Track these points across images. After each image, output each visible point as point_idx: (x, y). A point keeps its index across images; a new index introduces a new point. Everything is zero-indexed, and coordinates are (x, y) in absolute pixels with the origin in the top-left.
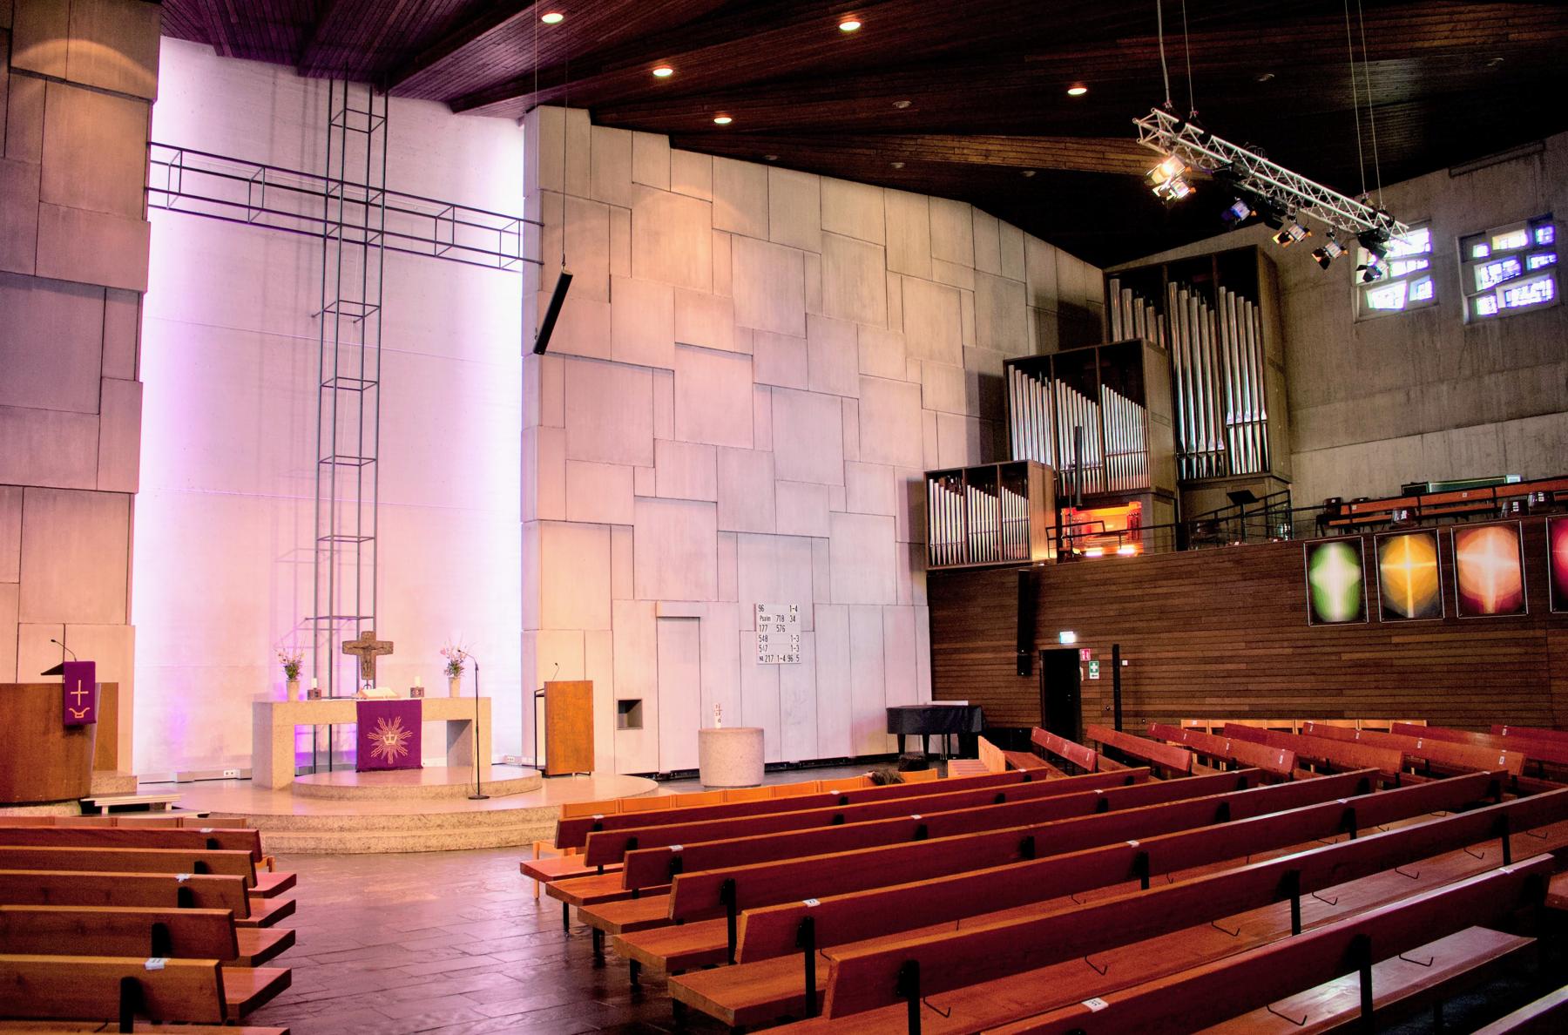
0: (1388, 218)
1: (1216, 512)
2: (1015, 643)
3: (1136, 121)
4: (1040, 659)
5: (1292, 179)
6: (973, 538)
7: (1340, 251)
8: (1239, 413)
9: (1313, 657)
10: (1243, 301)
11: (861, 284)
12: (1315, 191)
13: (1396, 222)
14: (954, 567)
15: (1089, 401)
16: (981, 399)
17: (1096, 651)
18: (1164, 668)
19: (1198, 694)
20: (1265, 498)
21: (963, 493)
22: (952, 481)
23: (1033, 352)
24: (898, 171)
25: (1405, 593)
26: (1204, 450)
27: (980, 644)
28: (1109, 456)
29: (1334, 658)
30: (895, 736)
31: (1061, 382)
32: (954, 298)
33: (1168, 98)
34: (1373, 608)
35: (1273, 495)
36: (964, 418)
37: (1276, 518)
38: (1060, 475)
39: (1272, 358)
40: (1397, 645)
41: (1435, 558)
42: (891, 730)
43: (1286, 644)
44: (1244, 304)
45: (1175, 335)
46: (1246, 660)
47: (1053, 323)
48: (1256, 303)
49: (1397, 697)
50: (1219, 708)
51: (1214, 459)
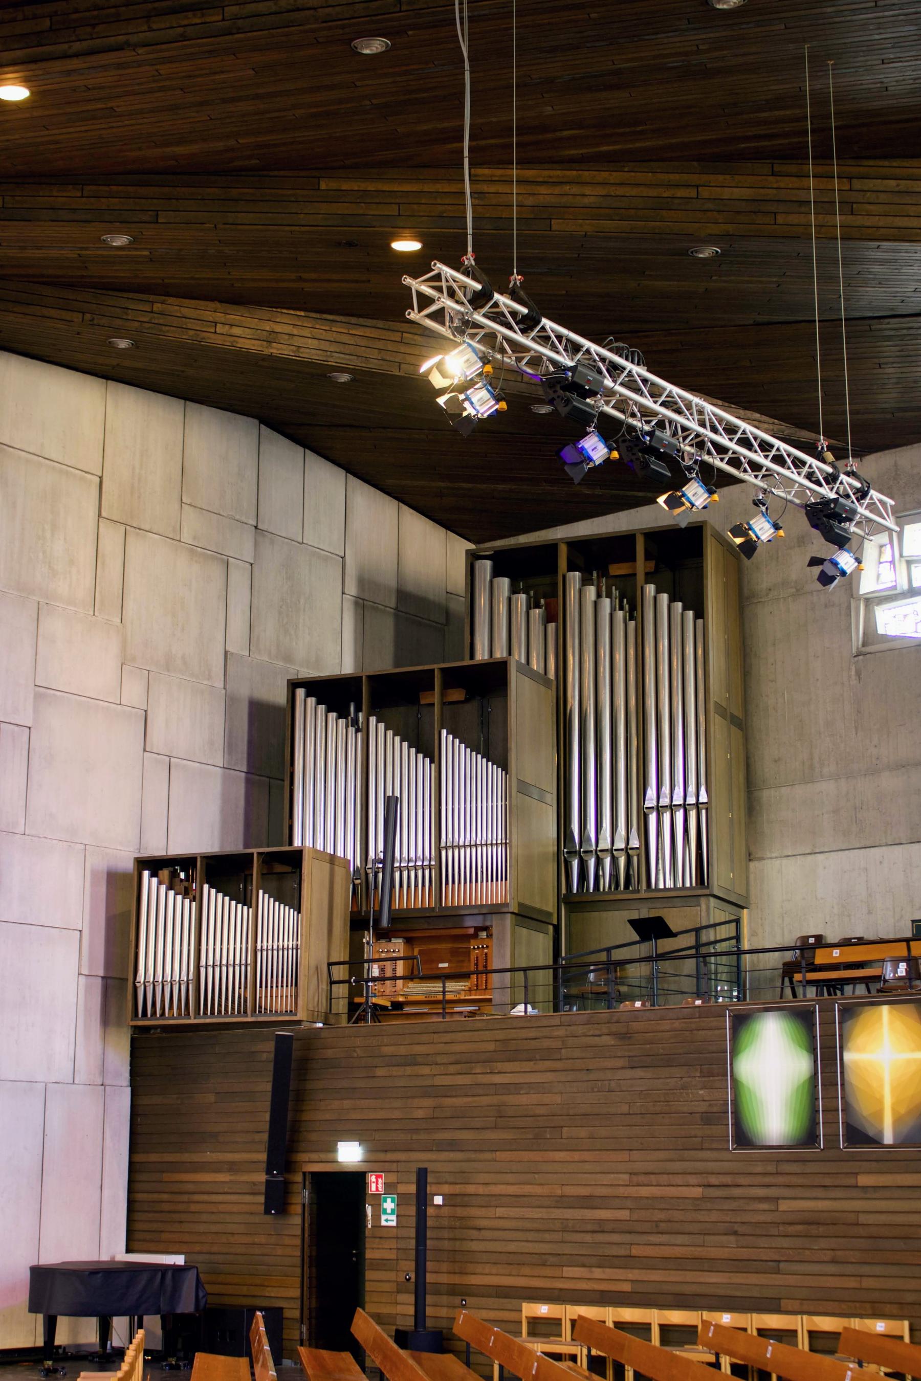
0: (858, 485)
1: (608, 950)
2: (263, 1157)
3: (408, 281)
4: (304, 1188)
5: (689, 406)
6: (208, 976)
7: (772, 530)
8: (666, 789)
9: (734, 1205)
10: (680, 610)
12: (731, 430)
13: (872, 492)
16: (250, 743)
17: (393, 1178)
18: (500, 1212)
19: (552, 1260)
21: (197, 899)
22: (182, 875)
23: (348, 667)
24: (123, 353)
25: (880, 1101)
26: (609, 846)
27: (210, 1156)
28: (446, 848)
30: (40, 1317)
31: (378, 721)
32: (216, 571)
33: (470, 249)
34: (831, 1123)
35: (715, 925)
36: (243, 775)
37: (716, 964)
38: (367, 874)
40: (865, 1188)
42: (34, 1307)
43: (693, 1180)
44: (682, 614)
45: (572, 661)
46: (629, 1204)
47: (386, 628)
48: (700, 614)
49: (864, 1279)
50: (584, 1286)
51: (622, 861)
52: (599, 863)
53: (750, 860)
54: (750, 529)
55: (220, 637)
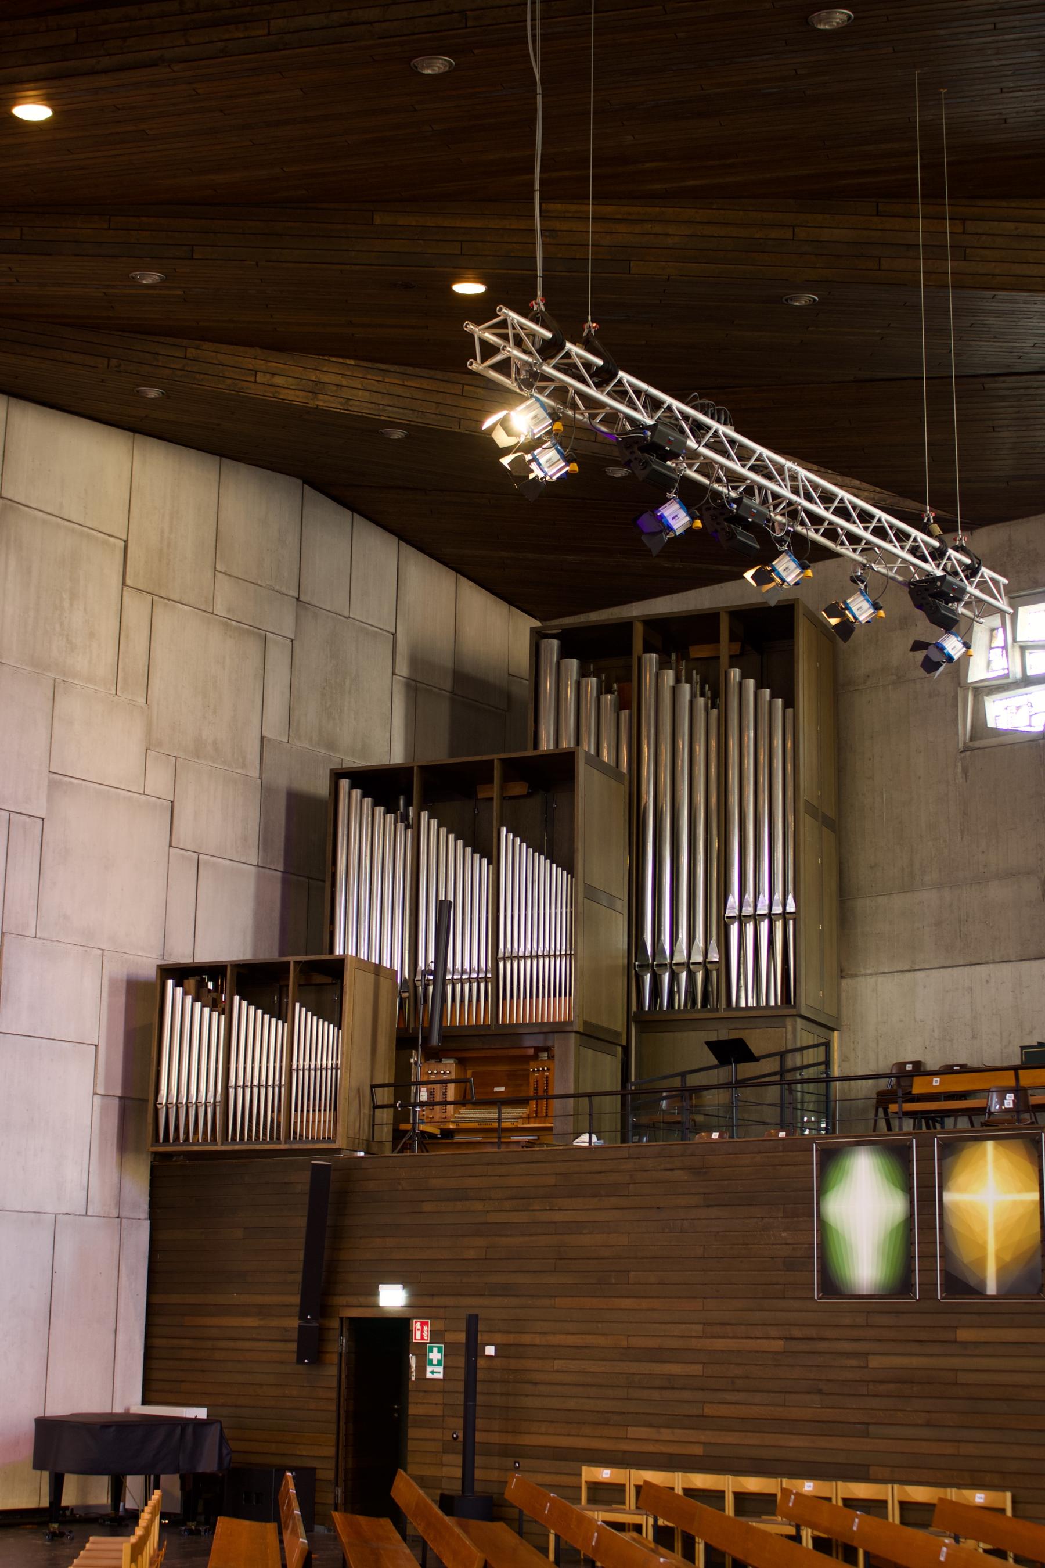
0: (968, 561)
1: (683, 1075)
2: (296, 1300)
3: (470, 327)
7: (871, 611)
8: (749, 897)
10: (768, 698)
11: (71, 605)
12: (827, 498)
13: (983, 569)
14: (196, 1148)
15: (477, 856)
17: (440, 1325)
18: (558, 1364)
20: (782, 1055)
21: (227, 1011)
22: (210, 986)
23: (398, 757)
25: (983, 1248)
27: (236, 1298)
28: (504, 959)
29: (853, 1362)
30: (46, 1474)
32: (253, 647)
33: (539, 293)
34: (928, 1270)
35: (801, 1049)
37: (803, 1092)
38: (416, 987)
39: (815, 803)
41: (1038, 1188)
42: (39, 1464)
43: (773, 1332)
44: (770, 703)
48: (790, 702)
50: (650, 1448)
51: (700, 976)
52: (674, 978)
53: (842, 977)
54: (848, 608)
55: (256, 720)
